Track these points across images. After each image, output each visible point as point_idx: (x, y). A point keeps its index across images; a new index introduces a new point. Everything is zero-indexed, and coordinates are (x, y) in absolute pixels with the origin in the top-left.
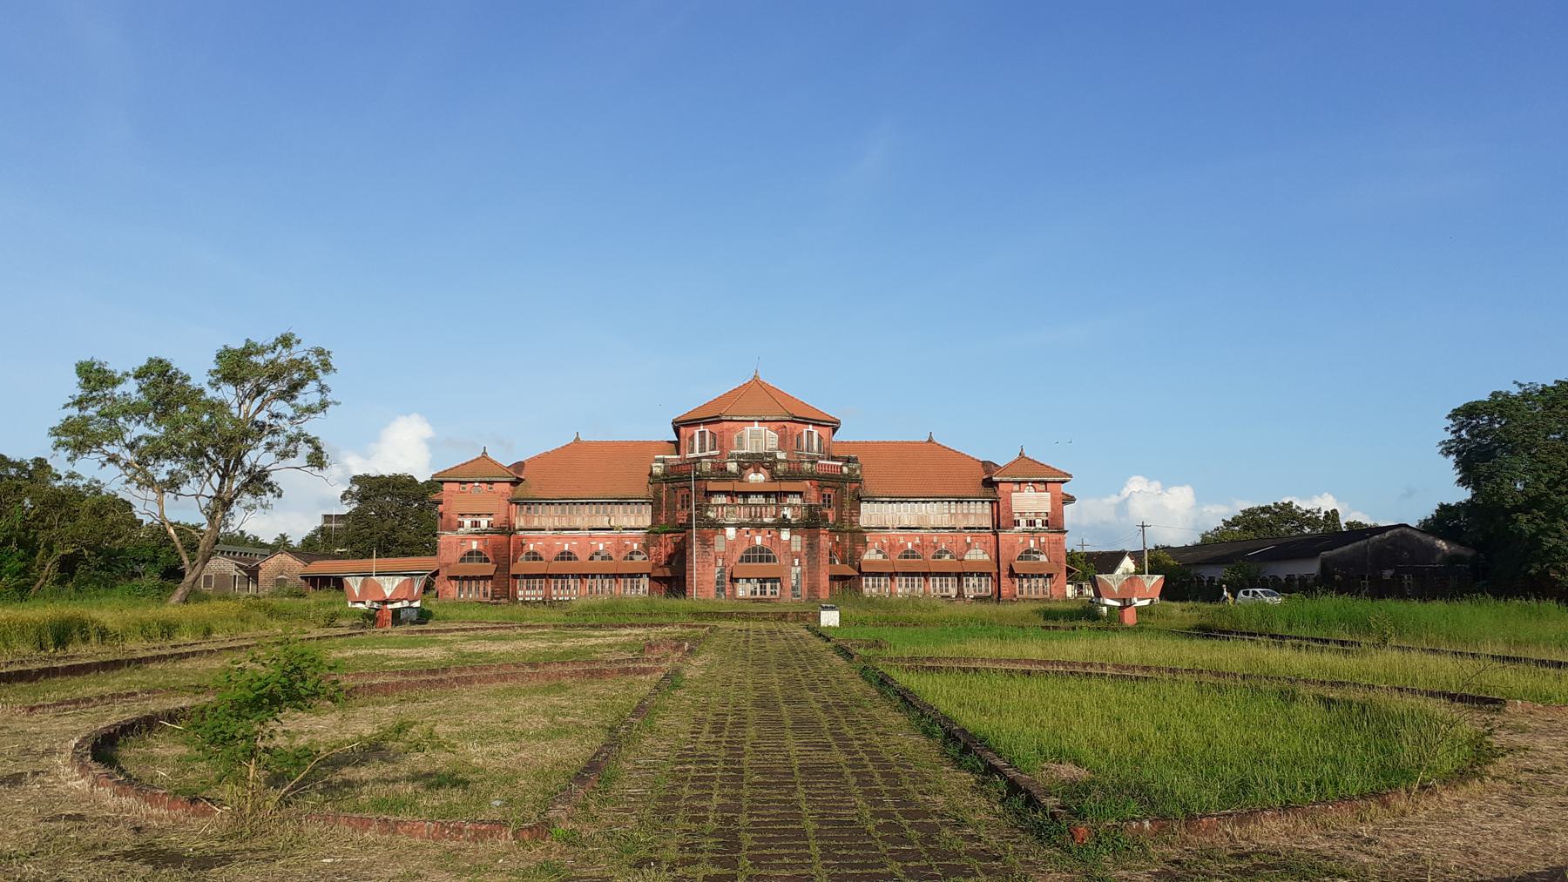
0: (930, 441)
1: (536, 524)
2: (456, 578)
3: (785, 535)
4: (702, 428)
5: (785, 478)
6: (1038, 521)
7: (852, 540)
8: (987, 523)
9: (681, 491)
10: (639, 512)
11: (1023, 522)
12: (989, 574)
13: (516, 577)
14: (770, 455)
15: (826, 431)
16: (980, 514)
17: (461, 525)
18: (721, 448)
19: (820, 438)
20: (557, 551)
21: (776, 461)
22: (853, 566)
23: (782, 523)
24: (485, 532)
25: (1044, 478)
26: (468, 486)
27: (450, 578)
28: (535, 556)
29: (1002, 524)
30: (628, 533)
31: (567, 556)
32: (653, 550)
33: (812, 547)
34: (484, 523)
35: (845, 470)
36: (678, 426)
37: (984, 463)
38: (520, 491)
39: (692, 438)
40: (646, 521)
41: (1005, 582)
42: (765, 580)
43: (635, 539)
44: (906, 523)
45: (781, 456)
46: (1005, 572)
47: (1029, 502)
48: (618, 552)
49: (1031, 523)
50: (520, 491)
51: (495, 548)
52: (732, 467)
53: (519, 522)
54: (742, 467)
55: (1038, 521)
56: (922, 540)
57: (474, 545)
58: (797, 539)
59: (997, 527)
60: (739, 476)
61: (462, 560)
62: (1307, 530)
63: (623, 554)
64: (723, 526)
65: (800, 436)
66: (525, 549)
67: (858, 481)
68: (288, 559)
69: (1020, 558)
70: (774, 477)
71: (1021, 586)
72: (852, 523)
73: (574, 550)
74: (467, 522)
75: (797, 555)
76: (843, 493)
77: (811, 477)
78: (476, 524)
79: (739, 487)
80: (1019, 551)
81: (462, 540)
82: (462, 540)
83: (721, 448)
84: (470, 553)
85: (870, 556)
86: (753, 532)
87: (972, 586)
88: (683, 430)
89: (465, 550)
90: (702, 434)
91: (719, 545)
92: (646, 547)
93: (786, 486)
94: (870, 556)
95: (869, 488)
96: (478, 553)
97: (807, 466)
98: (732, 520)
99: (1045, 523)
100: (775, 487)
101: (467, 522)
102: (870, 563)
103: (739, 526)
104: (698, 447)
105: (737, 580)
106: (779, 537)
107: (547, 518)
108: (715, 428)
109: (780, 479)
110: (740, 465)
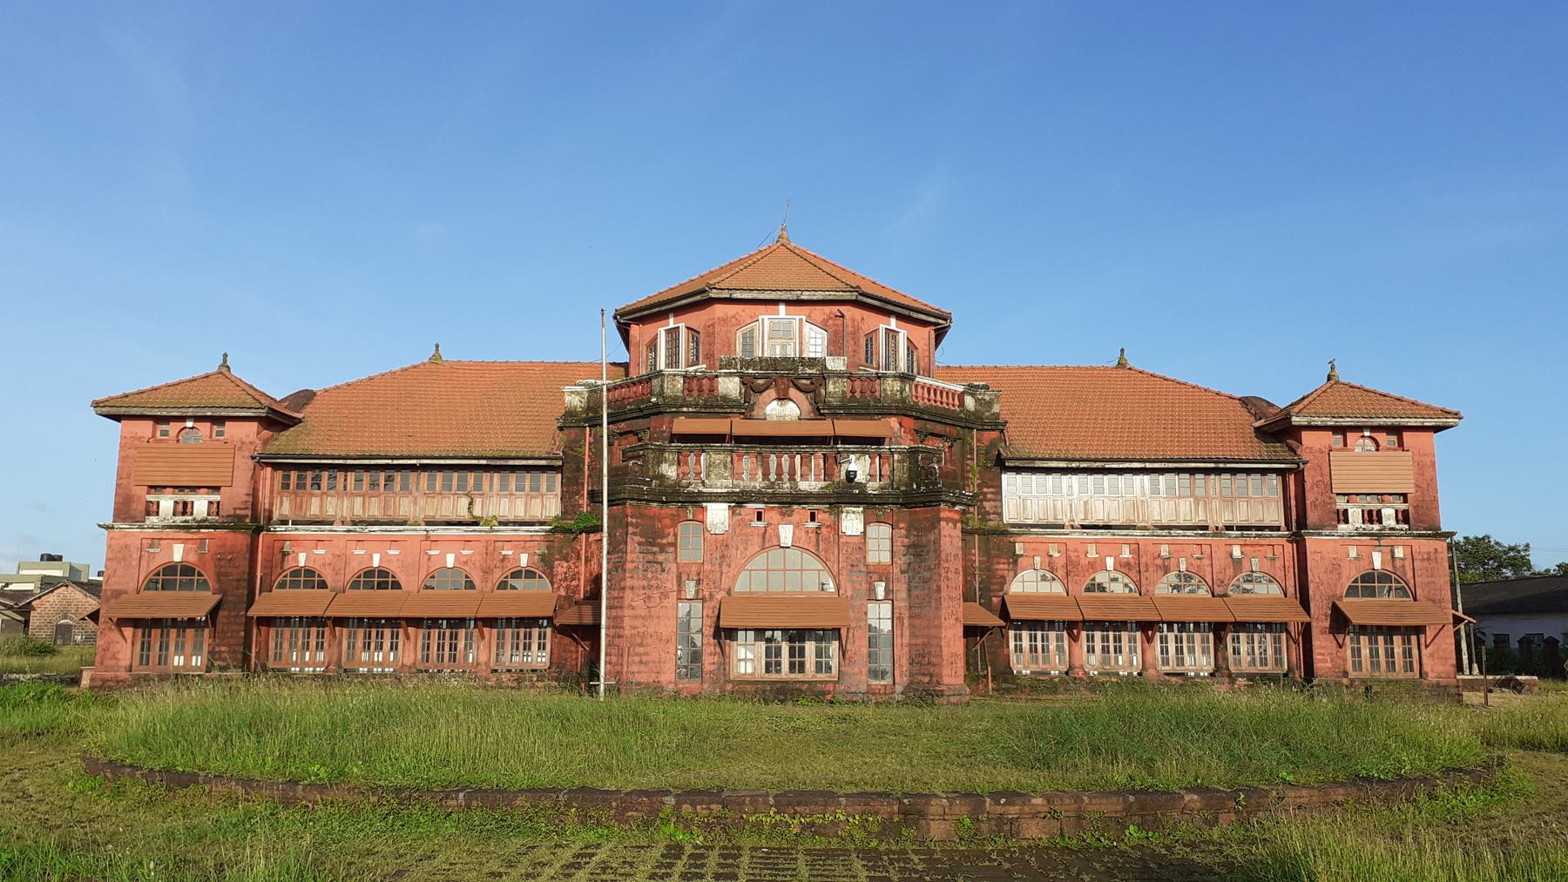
0: (1121, 365)
1: (314, 509)
2: (136, 623)
3: (852, 522)
4: (672, 322)
5: (847, 408)
6: (1388, 513)
7: (986, 552)
8: (1275, 516)
9: (624, 452)
10: (535, 488)
11: (1355, 514)
12: (1283, 626)
13: (267, 621)
14: (813, 362)
15: (923, 335)
16: (1261, 502)
17: (152, 509)
18: (710, 356)
19: (911, 347)
20: (355, 567)
21: (824, 376)
22: (988, 606)
23: (845, 495)
24: (201, 525)
25: (1397, 427)
26: (173, 428)
27: (122, 623)
28: (310, 578)
29: (1312, 516)
30: (508, 532)
31: (381, 579)
32: (561, 568)
33: (919, 552)
34: (201, 505)
35: (970, 402)
36: (627, 321)
37: (1245, 401)
38: (286, 442)
39: (653, 346)
40: (550, 506)
41: (1322, 644)
42: (797, 636)
43: (523, 545)
44: (1098, 517)
45: (836, 364)
46: (1320, 622)
47: (1357, 468)
48: (487, 571)
49: (1372, 517)
50: (286, 442)
51: (222, 561)
52: (730, 386)
53: (283, 508)
54: (751, 387)
55: (1388, 513)
56: (1137, 550)
57: (178, 553)
58: (881, 534)
59: (1298, 525)
60: (745, 407)
61: (152, 584)
62: (1508, 573)
63: (498, 576)
64: (697, 500)
65: (871, 338)
66: (289, 564)
67: (997, 425)
68: (77, 595)
69: (1352, 591)
70: (820, 410)
71: (1357, 652)
72: (984, 515)
73: (393, 568)
74: (167, 503)
75: (882, 573)
76: (966, 451)
77: (902, 410)
78: (185, 508)
79: (741, 427)
80: (1350, 575)
81: (153, 542)
82: (153, 542)
83: (710, 356)
84: (170, 569)
85: (1026, 584)
86: (772, 515)
87: (1246, 652)
88: (635, 330)
89: (159, 561)
90: (673, 333)
91: (689, 548)
92: (547, 562)
93: (847, 427)
94: (1026, 584)
95: (1019, 442)
96: (187, 570)
97: (892, 386)
98: (721, 484)
99: (1404, 517)
100: (824, 428)
101: (167, 503)
102: (1027, 600)
103: (737, 500)
104: (668, 353)
105: (731, 633)
106: (836, 527)
107: (338, 502)
108: (697, 319)
109: (835, 413)
110: (746, 382)
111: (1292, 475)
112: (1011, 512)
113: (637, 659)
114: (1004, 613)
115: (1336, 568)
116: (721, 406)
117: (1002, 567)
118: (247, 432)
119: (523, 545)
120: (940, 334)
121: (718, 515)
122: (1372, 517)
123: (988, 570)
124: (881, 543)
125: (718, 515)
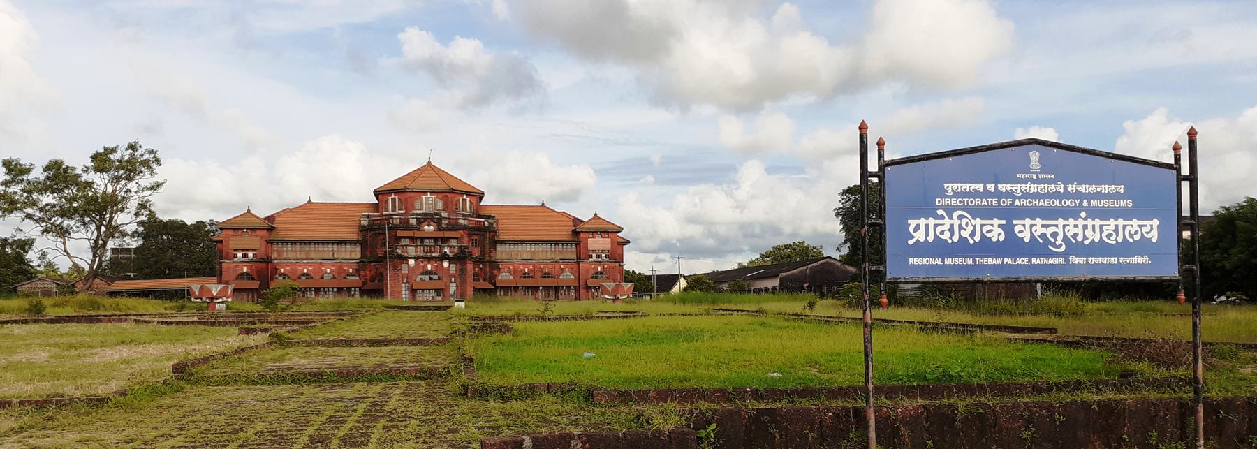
15: (474, 200)
17: (235, 256)
23: (444, 257)
24: (251, 261)
32: (362, 273)
33: (462, 272)
36: (377, 193)
43: (350, 266)
45: (445, 215)
49: (599, 256)
52: (413, 221)
54: (420, 222)
64: (406, 259)
70: (440, 228)
74: (240, 255)
78: (245, 256)
80: (591, 273)
84: (242, 274)
90: (393, 200)
93: (447, 234)
95: (503, 235)
96: (247, 274)
98: (413, 255)
99: (607, 257)
101: (240, 255)
103: (416, 259)
104: (392, 208)
108: (403, 196)
109: (444, 229)
111: (578, 244)
112: (498, 256)
113: (697, 200)
114: (494, 284)
115: (587, 271)
116: (411, 228)
117: (495, 272)
118: (264, 233)
119: (350, 266)
120: (481, 199)
121: (412, 262)
122: (599, 256)
123: (491, 272)
124: (453, 269)
125: (412, 262)
